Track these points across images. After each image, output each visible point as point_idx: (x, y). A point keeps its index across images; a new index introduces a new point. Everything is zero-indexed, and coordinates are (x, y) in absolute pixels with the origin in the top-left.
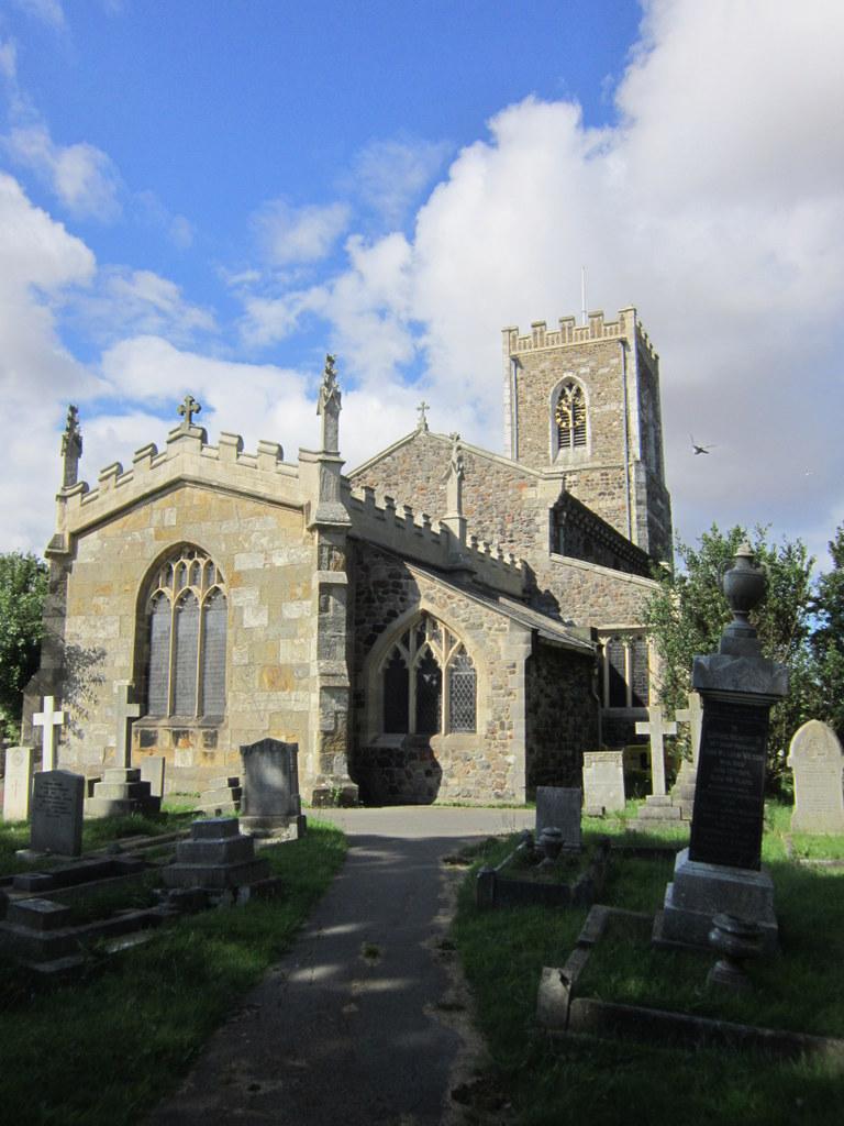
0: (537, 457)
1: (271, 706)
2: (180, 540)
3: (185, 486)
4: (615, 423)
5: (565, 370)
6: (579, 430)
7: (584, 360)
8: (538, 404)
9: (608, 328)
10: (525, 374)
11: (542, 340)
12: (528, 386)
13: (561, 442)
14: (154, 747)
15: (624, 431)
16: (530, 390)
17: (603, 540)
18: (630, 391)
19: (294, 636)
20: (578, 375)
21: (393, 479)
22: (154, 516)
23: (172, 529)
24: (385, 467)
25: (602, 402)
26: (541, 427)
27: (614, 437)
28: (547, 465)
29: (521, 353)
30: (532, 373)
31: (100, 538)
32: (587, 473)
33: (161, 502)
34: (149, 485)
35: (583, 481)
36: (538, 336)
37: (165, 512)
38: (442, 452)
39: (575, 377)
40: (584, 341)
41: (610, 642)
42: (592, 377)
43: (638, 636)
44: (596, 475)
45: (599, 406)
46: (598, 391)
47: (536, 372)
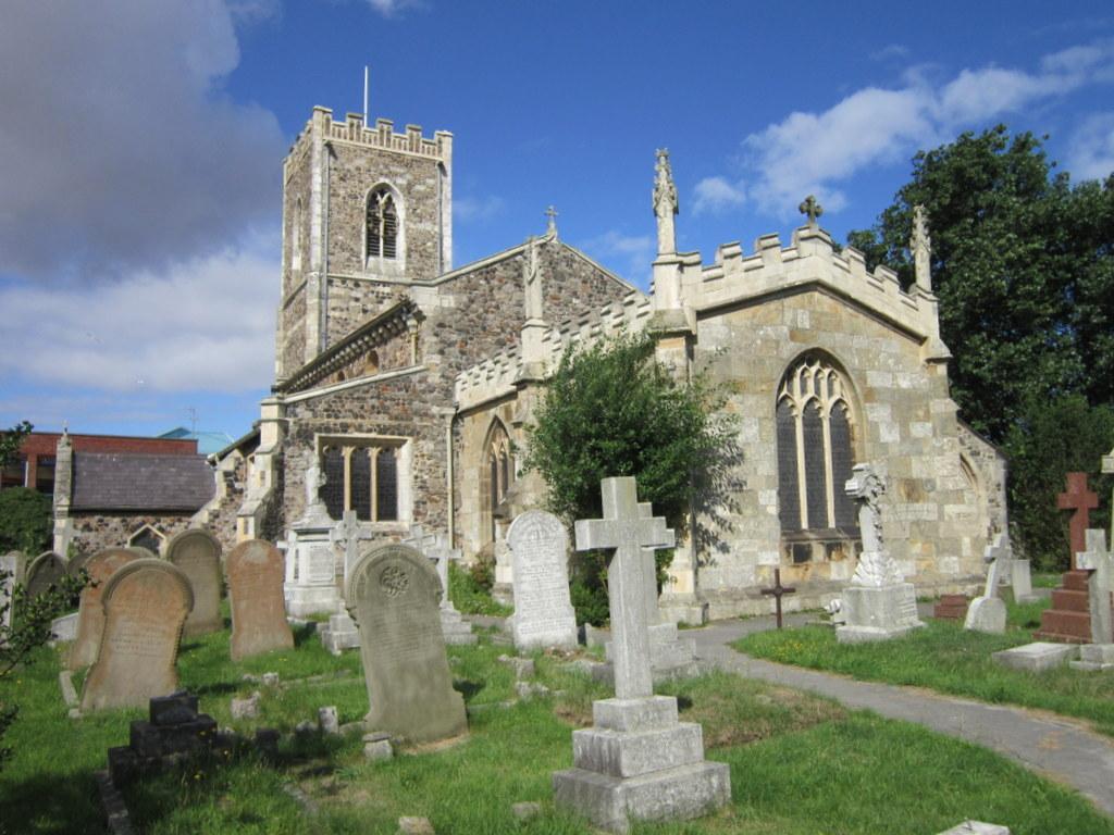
0: (349, 260)
1: (910, 517)
2: (816, 346)
3: (816, 290)
4: (429, 244)
5: (382, 174)
6: (390, 241)
8: (351, 202)
9: (426, 146)
10: (338, 165)
11: (358, 134)
12: (342, 179)
13: (372, 250)
14: (809, 562)
15: (438, 254)
16: (343, 184)
17: (347, 358)
18: (444, 216)
19: (921, 453)
20: (395, 183)
22: (786, 314)
23: (808, 332)
24: (516, 266)
25: (417, 219)
26: (354, 228)
27: (428, 257)
28: (359, 270)
29: (336, 141)
32: (401, 287)
33: (790, 301)
34: (781, 279)
36: (355, 128)
37: (796, 312)
38: (575, 266)
39: (391, 184)
40: (402, 151)
41: (380, 452)
42: (408, 190)
43: (388, 449)
45: (415, 223)
46: (414, 206)
47: (352, 168)
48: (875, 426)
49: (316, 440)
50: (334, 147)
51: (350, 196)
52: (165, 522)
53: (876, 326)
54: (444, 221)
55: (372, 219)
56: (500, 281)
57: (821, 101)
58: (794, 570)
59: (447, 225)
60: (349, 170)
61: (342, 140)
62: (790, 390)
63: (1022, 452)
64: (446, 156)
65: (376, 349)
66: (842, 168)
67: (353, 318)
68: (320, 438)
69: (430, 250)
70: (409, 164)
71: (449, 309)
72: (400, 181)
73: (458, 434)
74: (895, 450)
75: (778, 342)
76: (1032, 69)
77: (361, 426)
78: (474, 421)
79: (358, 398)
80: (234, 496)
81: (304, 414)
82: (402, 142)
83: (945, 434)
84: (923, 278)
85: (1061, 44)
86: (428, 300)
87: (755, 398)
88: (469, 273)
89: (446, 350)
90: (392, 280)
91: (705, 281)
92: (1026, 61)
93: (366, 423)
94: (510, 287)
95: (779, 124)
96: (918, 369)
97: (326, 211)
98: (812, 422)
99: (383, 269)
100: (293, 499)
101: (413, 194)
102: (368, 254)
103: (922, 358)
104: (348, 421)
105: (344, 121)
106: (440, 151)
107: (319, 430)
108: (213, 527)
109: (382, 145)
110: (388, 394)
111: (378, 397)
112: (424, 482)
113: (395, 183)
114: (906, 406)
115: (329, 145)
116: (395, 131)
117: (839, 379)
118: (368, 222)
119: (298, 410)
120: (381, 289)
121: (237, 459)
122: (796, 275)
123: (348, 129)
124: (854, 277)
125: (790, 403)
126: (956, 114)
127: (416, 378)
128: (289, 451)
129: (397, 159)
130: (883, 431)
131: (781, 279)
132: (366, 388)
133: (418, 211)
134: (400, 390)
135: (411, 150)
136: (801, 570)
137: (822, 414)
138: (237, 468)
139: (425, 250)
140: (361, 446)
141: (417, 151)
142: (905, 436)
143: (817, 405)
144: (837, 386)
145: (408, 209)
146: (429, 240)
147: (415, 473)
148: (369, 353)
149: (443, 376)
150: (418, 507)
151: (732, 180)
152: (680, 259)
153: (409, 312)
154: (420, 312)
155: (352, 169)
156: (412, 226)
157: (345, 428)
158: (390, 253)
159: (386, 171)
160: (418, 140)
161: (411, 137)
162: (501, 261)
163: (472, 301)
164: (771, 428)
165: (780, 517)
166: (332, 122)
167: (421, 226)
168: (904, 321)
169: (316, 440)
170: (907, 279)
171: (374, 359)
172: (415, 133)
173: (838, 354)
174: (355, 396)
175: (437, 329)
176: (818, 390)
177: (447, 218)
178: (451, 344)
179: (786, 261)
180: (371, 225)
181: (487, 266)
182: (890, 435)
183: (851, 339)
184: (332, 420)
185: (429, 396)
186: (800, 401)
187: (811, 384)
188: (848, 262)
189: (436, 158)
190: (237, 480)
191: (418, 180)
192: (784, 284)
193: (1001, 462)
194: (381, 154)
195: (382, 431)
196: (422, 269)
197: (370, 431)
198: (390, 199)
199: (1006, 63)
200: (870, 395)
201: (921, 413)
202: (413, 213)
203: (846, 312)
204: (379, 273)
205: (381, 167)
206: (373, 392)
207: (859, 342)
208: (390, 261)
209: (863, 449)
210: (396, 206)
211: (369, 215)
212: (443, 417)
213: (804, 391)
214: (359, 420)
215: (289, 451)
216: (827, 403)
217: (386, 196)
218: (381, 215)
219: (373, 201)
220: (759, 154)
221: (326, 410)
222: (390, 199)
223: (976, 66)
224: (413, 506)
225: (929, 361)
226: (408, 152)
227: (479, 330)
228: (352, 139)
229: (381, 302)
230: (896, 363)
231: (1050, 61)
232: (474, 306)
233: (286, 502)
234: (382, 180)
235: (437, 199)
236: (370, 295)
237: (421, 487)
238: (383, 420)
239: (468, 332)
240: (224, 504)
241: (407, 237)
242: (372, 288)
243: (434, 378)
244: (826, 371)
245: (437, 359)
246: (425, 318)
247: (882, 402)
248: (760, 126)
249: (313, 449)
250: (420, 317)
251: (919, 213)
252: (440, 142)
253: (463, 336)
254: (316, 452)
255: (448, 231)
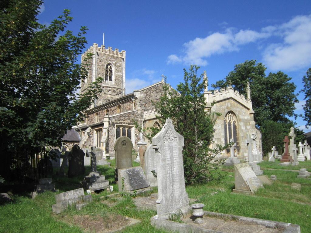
4: (120, 78)
5: (109, 60)
6: (111, 77)
7: (114, 60)
8: (102, 67)
10: (99, 58)
11: (104, 50)
12: (100, 61)
13: (107, 79)
18: (123, 71)
20: (112, 63)
21: (157, 91)
26: (103, 73)
29: (99, 52)
30: (101, 58)
31: (216, 106)
32: (114, 88)
33: (226, 101)
35: (112, 90)
36: (103, 49)
37: (228, 103)
40: (114, 55)
42: (115, 64)
43: (130, 128)
44: (115, 90)
48: (241, 126)
49: (116, 125)
50: (98, 54)
51: (102, 66)
52: (68, 144)
53: (241, 106)
54: (123, 72)
55: (107, 71)
56: (153, 91)
57: (204, 35)
58: (227, 154)
59: (124, 74)
60: (102, 59)
61: (100, 52)
62: (226, 119)
63: (264, 132)
64: (124, 57)
65: (120, 105)
66: (207, 54)
67: (102, 95)
68: (116, 125)
69: (120, 79)
70: (116, 58)
71: (142, 97)
72: (113, 62)
73: (144, 125)
74: (244, 131)
75: (224, 109)
76: (258, 30)
77: (125, 123)
78: (149, 122)
79: (124, 117)
80: (90, 138)
81: (113, 120)
82: (114, 53)
83: (253, 128)
84: (249, 97)
85: (266, 25)
86: (138, 95)
87: (221, 120)
88: (146, 89)
89: (142, 106)
90: (111, 86)
91: (213, 97)
92: (258, 29)
93: (126, 122)
94: (154, 92)
95: (193, 41)
96: (248, 115)
97: (96, 69)
98: (230, 125)
99: (109, 84)
100: (111, 139)
101: (117, 66)
102: (106, 80)
103: (249, 113)
104: (122, 121)
105: (101, 47)
106: (123, 55)
107: (116, 123)
108: (85, 145)
109: (109, 53)
110: (130, 116)
111: (128, 116)
112: (137, 135)
113: (112, 63)
114: (246, 122)
115: (97, 53)
116: (113, 50)
117: (234, 117)
118: (106, 72)
119: (112, 119)
120: (109, 88)
121: (90, 129)
122: (228, 96)
123: (102, 49)
124: (235, 95)
125: (226, 121)
126: (238, 41)
127: (136, 112)
128: (110, 128)
129: (113, 57)
130: (242, 127)
131: (225, 97)
132: (126, 114)
133: (118, 70)
134: (132, 115)
135: (116, 55)
136: (228, 154)
137: (231, 124)
138: (90, 132)
139: (119, 79)
140: (124, 127)
141: (118, 55)
142: (246, 128)
143: (230, 122)
144: (234, 118)
145: (115, 69)
146: (120, 77)
147: (135, 133)
148: (118, 105)
149: (141, 112)
150: (136, 141)
151: (178, 55)
152: (209, 93)
153: (133, 97)
154: (136, 97)
155: (103, 59)
156: (116, 73)
157: (121, 123)
158: (111, 80)
159: (110, 60)
160: (118, 53)
161: (116, 52)
162: (153, 86)
163: (147, 95)
164: (223, 126)
165: (225, 143)
166: (98, 47)
167: (118, 74)
168: (246, 105)
169: (116, 125)
170: (246, 97)
171: (120, 107)
172: (117, 51)
173: (235, 112)
174: (124, 116)
175: (140, 101)
176: (231, 119)
177: (124, 72)
178: (143, 105)
179: (226, 93)
180: (106, 73)
181: (150, 88)
182: (243, 128)
183: (237, 109)
184: (119, 121)
185: (138, 116)
186: (228, 121)
187: (229, 117)
188: (236, 93)
189: (122, 57)
190: (90, 134)
191: (118, 62)
192: (226, 98)
193: (261, 134)
194: (109, 56)
195: (129, 124)
196: (118, 84)
197: (126, 124)
198: (111, 66)
199: (252, 29)
200: (240, 120)
201: (248, 124)
202: (116, 70)
203: (236, 103)
204: (108, 85)
205: (109, 59)
206: (127, 115)
207: (238, 109)
208: (111, 82)
209: (238, 131)
210: (112, 68)
211: (106, 70)
212: (141, 121)
213: (228, 119)
214: (124, 121)
215: (110, 128)
216: (232, 121)
217: (110, 66)
218: (109, 70)
219: (107, 67)
220: (187, 49)
221: (118, 119)
222: (111, 66)
223: (244, 29)
224: (135, 141)
225: (250, 113)
226: (115, 55)
227: (148, 102)
228: (104, 52)
229: (109, 92)
230: (244, 114)
231: (263, 29)
232: (147, 96)
233: (109, 140)
234: (109, 62)
235: (122, 67)
236: (106, 90)
237: (137, 137)
238: (129, 121)
239: (146, 102)
240: (87, 140)
241: (115, 76)
242: (107, 88)
243: (139, 112)
244: (232, 115)
245: (140, 108)
246: (137, 99)
247: (242, 121)
248: (188, 41)
249: (115, 128)
250: (136, 99)
251: (248, 84)
252: (123, 53)
253: (145, 103)
254: (115, 128)
255: (124, 75)
